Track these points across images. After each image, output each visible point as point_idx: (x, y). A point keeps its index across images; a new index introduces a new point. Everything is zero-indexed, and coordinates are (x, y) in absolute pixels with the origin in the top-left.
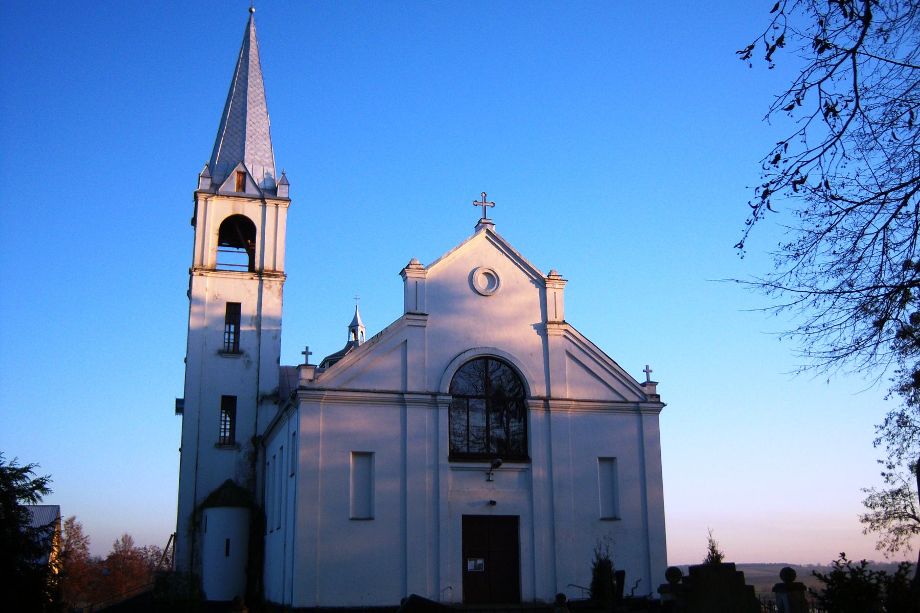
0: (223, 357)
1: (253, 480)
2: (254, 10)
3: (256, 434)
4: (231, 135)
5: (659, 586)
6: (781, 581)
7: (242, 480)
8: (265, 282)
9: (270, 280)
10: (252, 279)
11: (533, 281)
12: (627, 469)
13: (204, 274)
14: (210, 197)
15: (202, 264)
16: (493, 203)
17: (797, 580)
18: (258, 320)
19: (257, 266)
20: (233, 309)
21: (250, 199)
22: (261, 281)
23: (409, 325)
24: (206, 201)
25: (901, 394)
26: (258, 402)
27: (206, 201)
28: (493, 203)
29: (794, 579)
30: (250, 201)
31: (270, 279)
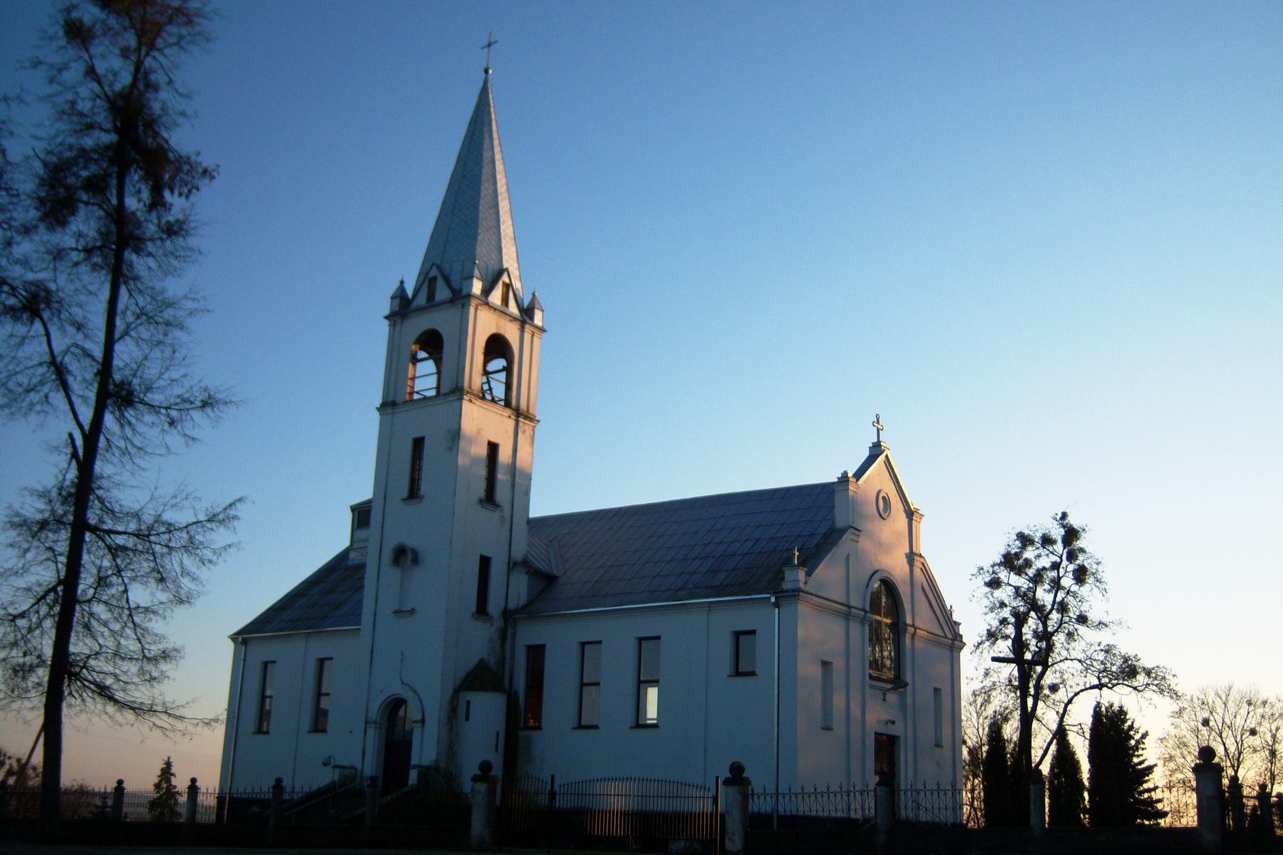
0: (483, 507)
1: (502, 661)
2: (490, 71)
3: (506, 606)
4: (487, 230)
5: (472, 776)
6: (478, 772)
7: (492, 661)
8: (521, 424)
9: (525, 423)
10: (510, 417)
11: (905, 511)
12: (946, 691)
13: (473, 401)
14: (480, 305)
15: (470, 387)
16: (874, 426)
17: (745, 775)
18: (513, 468)
19: (514, 402)
20: (493, 448)
21: (511, 318)
22: (517, 422)
23: (852, 539)
24: (476, 309)
25: (1108, 645)
26: (509, 569)
27: (476, 309)
28: (874, 426)
29: (729, 778)
30: (511, 321)
31: (526, 422)
